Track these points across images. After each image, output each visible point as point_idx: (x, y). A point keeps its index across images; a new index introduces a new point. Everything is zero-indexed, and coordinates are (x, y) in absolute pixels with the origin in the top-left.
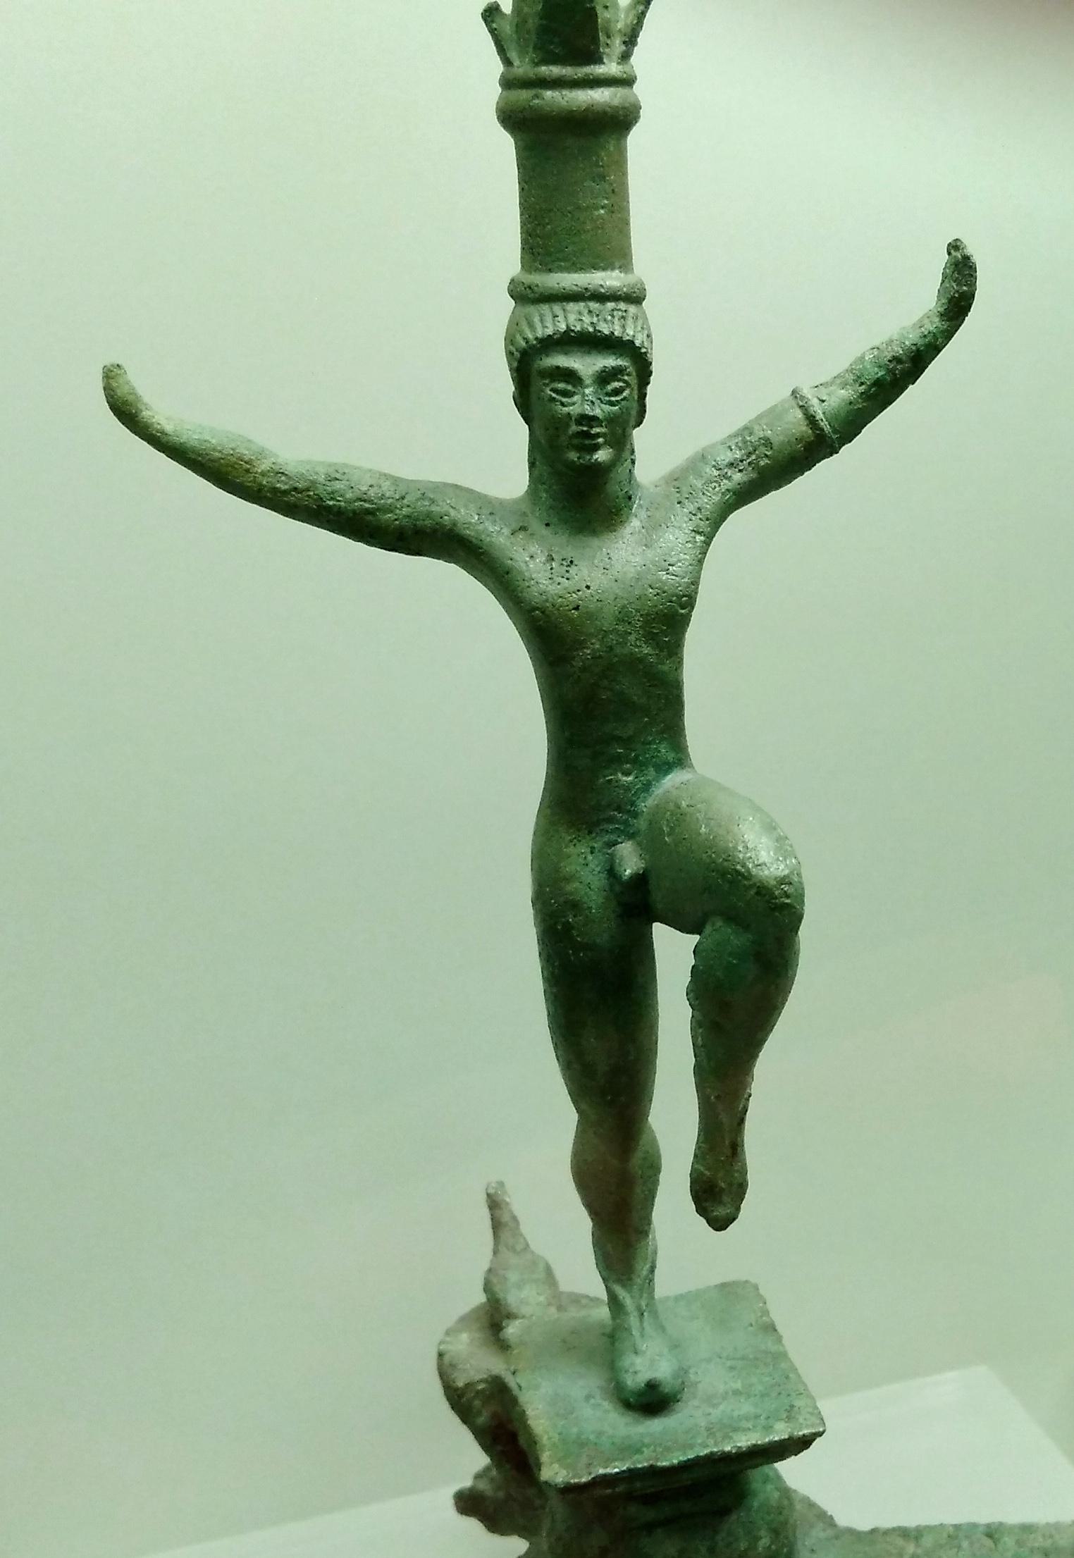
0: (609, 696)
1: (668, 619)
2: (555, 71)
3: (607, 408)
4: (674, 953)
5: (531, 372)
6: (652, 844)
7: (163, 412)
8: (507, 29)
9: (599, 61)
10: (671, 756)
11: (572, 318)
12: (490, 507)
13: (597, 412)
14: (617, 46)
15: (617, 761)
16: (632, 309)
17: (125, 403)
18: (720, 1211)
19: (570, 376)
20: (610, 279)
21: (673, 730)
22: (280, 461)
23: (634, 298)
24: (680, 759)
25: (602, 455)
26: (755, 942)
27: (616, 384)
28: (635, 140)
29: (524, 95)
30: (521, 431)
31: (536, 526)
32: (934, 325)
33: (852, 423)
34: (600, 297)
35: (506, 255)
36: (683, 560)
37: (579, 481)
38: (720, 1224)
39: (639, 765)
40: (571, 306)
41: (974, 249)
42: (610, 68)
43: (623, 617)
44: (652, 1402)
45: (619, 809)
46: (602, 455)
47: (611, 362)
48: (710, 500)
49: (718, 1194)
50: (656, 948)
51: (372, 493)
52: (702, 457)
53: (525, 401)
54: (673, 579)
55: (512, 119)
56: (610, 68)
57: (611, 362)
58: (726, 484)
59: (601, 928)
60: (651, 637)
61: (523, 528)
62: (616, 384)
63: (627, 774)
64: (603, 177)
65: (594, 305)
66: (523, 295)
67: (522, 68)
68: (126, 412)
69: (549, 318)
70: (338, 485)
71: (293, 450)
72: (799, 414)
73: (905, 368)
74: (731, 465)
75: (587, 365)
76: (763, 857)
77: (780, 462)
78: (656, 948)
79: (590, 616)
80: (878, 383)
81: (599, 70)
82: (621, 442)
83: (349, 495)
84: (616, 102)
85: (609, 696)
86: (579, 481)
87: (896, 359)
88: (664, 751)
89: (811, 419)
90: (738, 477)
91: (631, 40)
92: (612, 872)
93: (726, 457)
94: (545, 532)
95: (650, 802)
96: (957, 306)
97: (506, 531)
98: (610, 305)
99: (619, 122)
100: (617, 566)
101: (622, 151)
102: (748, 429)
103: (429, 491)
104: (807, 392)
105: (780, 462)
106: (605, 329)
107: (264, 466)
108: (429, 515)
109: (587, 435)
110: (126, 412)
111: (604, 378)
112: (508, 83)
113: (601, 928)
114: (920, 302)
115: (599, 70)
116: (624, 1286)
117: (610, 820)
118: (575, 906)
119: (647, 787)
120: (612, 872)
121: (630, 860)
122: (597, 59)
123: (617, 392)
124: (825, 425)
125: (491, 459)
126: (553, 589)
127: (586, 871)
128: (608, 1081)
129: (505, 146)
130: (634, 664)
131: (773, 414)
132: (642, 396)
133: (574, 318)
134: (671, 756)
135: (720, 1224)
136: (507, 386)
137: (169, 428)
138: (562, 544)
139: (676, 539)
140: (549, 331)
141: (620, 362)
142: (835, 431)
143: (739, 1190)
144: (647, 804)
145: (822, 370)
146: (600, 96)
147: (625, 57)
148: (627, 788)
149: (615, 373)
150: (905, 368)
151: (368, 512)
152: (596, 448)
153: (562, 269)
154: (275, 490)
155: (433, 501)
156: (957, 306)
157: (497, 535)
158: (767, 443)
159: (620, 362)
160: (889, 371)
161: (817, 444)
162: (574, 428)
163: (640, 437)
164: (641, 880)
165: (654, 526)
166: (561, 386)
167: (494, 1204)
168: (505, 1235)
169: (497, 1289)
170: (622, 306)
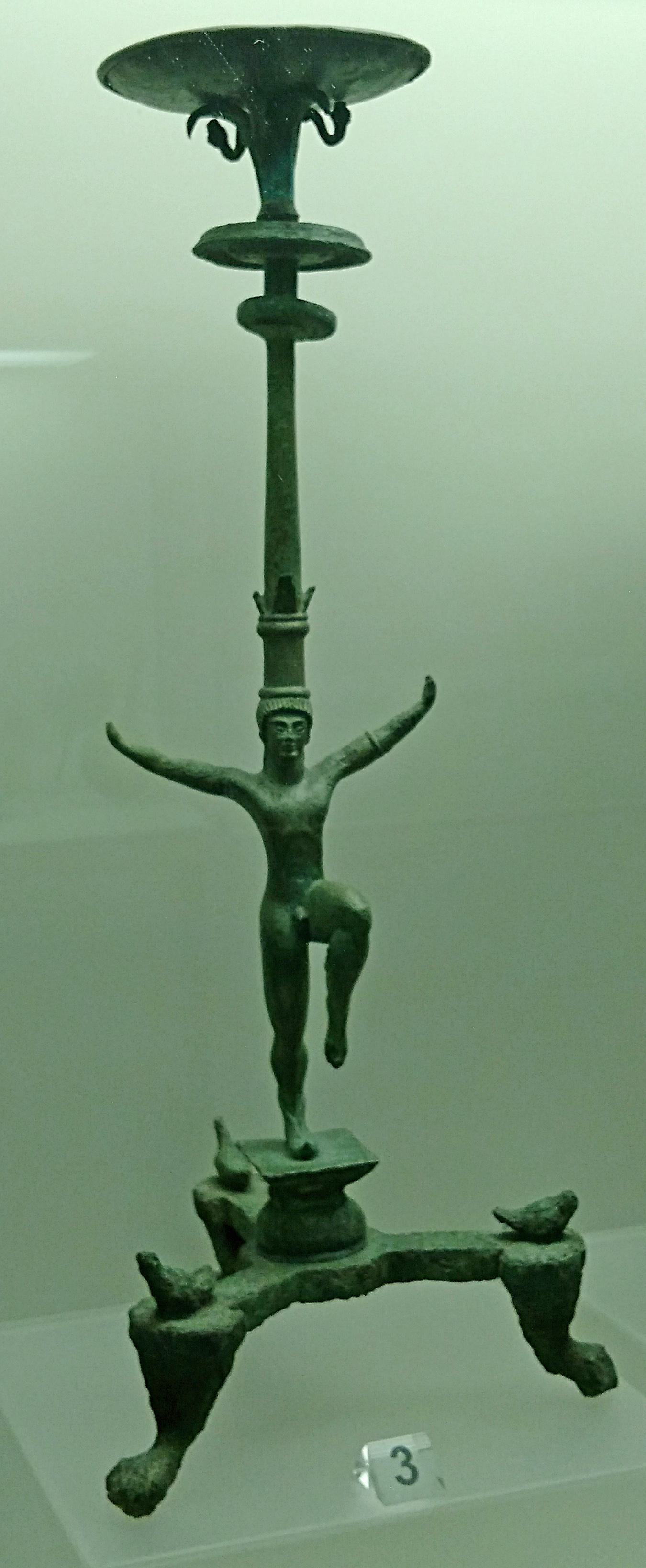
0: (292, 847)
1: (318, 816)
2: (280, 616)
4: (317, 953)
5: (267, 724)
6: (311, 906)
7: (127, 740)
8: (262, 601)
11: (285, 703)
12: (248, 776)
14: (302, 606)
16: (306, 700)
18: (338, 1059)
19: (283, 725)
21: (318, 863)
23: (306, 696)
24: (319, 875)
25: (294, 753)
26: (350, 936)
28: (307, 639)
29: (267, 625)
30: (262, 745)
31: (267, 782)
32: (419, 708)
33: (388, 745)
35: (259, 682)
36: (323, 795)
37: (283, 765)
38: (337, 1065)
41: (436, 679)
42: (300, 614)
43: (300, 817)
44: (307, 1153)
46: (294, 753)
47: (298, 719)
48: (334, 772)
49: (335, 1052)
50: (310, 944)
53: (263, 736)
54: (320, 802)
55: (262, 632)
56: (300, 614)
57: (298, 719)
58: (340, 768)
59: (288, 939)
65: (292, 698)
66: (263, 695)
67: (267, 614)
68: (114, 740)
69: (270, 704)
71: (172, 753)
75: (289, 720)
76: (357, 904)
77: (359, 760)
78: (310, 944)
82: (300, 750)
85: (292, 847)
86: (283, 765)
87: (406, 720)
88: (315, 871)
89: (372, 742)
90: (344, 765)
91: (306, 604)
92: (294, 918)
93: (339, 757)
94: (270, 785)
95: (310, 889)
96: (429, 700)
100: (298, 796)
101: (302, 643)
102: (347, 747)
103: (223, 771)
104: (371, 732)
105: (359, 760)
106: (297, 707)
107: (163, 760)
110: (114, 740)
111: (295, 725)
112: (261, 620)
113: (288, 939)
114: (416, 699)
116: (293, 1115)
118: (280, 933)
120: (294, 918)
121: (302, 913)
122: (294, 611)
123: (300, 730)
124: (378, 744)
125: (248, 758)
127: (283, 918)
128: (287, 1016)
129: (260, 641)
130: (305, 834)
131: (358, 741)
132: (308, 733)
133: (284, 703)
135: (337, 1065)
136: (257, 730)
139: (321, 786)
140: (276, 708)
143: (344, 1053)
144: (308, 891)
145: (377, 726)
146: (296, 624)
147: (305, 611)
156: (429, 700)
157: (252, 787)
158: (355, 751)
161: (376, 752)
162: (284, 743)
163: (307, 748)
164: (305, 921)
165: (310, 784)
166: (280, 728)
167: (218, 1127)
168: (224, 1140)
169: (223, 1161)
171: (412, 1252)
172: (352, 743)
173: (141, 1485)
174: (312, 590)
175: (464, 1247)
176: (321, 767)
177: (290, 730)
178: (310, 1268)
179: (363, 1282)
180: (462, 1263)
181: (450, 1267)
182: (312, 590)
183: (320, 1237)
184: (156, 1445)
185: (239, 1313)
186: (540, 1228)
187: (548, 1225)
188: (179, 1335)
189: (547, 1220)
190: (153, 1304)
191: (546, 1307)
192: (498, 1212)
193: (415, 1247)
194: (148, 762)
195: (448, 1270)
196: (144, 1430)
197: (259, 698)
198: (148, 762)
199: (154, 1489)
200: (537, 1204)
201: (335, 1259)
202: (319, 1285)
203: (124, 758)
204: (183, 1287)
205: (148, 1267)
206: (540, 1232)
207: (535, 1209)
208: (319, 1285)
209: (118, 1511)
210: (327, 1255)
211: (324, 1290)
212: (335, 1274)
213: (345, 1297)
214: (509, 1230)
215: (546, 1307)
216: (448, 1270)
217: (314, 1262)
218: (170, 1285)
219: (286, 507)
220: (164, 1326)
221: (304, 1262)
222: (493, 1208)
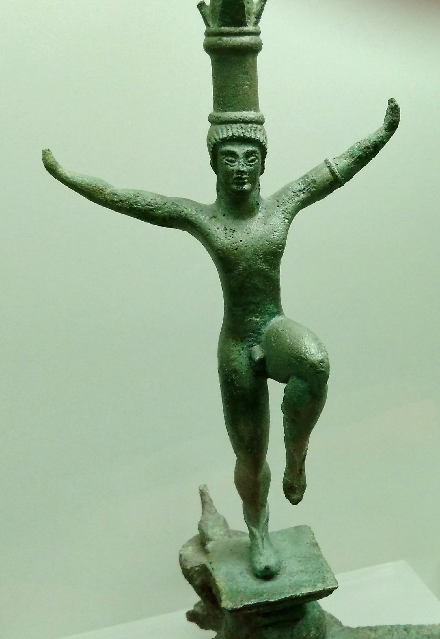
0: (250, 286)
1: (274, 254)
2: (228, 29)
3: (249, 167)
4: (276, 391)
5: (218, 152)
6: (267, 346)
7: (67, 169)
8: (208, 12)
9: (245, 25)
10: (275, 310)
11: (234, 130)
12: (201, 208)
13: (245, 169)
14: (253, 19)
15: (253, 312)
16: (259, 127)
17: (51, 165)
18: (295, 497)
19: (234, 154)
20: (250, 115)
21: (276, 299)
22: (115, 189)
23: (260, 122)
24: (279, 311)
25: (247, 187)
27: (252, 158)
28: (260, 57)
29: (215, 39)
30: (213, 177)
31: (220, 216)
32: (382, 133)
33: (349, 174)
34: (246, 122)
35: (207, 105)
36: (280, 230)
37: (237, 197)
38: (295, 502)
39: (262, 314)
40: (234, 126)
41: (399, 102)
42: (250, 28)
43: (255, 253)
44: (267, 575)
45: (254, 332)
46: (247, 187)
47: (250, 148)
48: (291, 205)
49: (294, 490)
50: (269, 389)
51: (152, 202)
52: (288, 188)
53: (215, 165)
54: (276, 238)
55: (210, 49)
56: (250, 28)
57: (250, 148)
58: (297, 199)
59: (246, 381)
60: (267, 261)
61: (214, 217)
62: (252, 158)
63: (257, 317)
64: (247, 73)
65: (243, 125)
66: (214, 121)
67: (214, 28)
68: (52, 169)
69: (225, 131)
70: (138, 199)
71: (120, 185)
72: (327, 170)
73: (371, 151)
74: (300, 191)
75: (240, 150)
76: (313, 351)
77: (319, 189)
78: (269, 389)
79: (242, 253)
80: (360, 157)
81: (246, 29)
82: (254, 181)
83: (143, 203)
84: (252, 42)
85: (250, 286)
86: (237, 197)
87: (367, 147)
88: (272, 308)
89: (332, 172)
90: (302, 196)
91: (258, 16)
92: (251, 358)
93: (297, 187)
94: (223, 218)
95: (266, 329)
96: (392, 126)
97: (207, 218)
98: (250, 125)
99: (254, 50)
100: (253, 232)
101: (255, 62)
102: (306, 176)
103: (176, 202)
104: (330, 161)
105: (319, 189)
106: (248, 135)
107: (108, 191)
108: (176, 211)
109: (240, 178)
110: (52, 169)
111: (247, 155)
112: (208, 34)
113: (246, 381)
114: (377, 124)
115: (246, 29)
116: (256, 527)
117: (250, 336)
118: (236, 372)
119: (265, 323)
120: (251, 358)
121: (258, 353)
122: (245, 24)
123: (253, 161)
124: (338, 174)
125: (201, 188)
126: (226, 242)
127: (240, 357)
128: (249, 444)
129: (207, 60)
130: (260, 272)
131: (317, 170)
132: (263, 162)
133: (235, 130)
134: (275, 310)
135: (295, 502)
136: (208, 158)
137: (69, 175)
138: (230, 223)
139: (277, 221)
140: (225, 136)
141: (254, 149)
142: (342, 177)
143: (303, 488)
144: (265, 330)
145: (337, 152)
146: (246, 39)
147: (256, 23)
148: (257, 323)
149: (252, 153)
150: (371, 151)
151: (151, 210)
152: (244, 184)
153: (230, 111)
154: (113, 201)
155: (177, 206)
156: (392, 126)
157: (204, 219)
158: (314, 182)
159: (254, 149)
160: (364, 152)
161: (335, 182)
162: (235, 176)
163: (262, 179)
164: (262, 361)
165: (268, 216)
166: (230, 158)
167: (202, 494)
168: (207, 507)
169: (204, 528)
170: (255, 125)
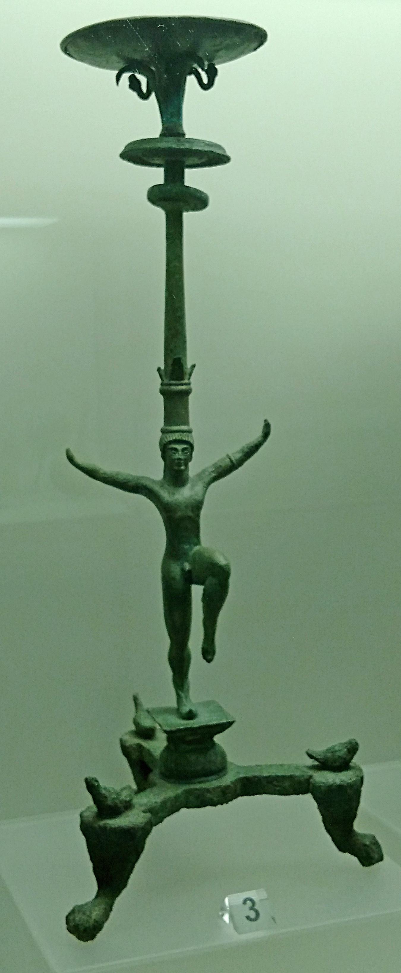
0: (181, 526)
1: (197, 506)
2: (174, 382)
4: (197, 591)
5: (166, 449)
6: (193, 562)
7: (79, 459)
8: (163, 373)
11: (177, 436)
12: (154, 481)
14: (187, 376)
16: (190, 434)
18: (210, 657)
19: (176, 450)
21: (198, 535)
23: (190, 432)
24: (198, 543)
25: (183, 468)
28: (191, 397)
29: (166, 388)
30: (162, 463)
31: (166, 485)
32: (260, 439)
33: (241, 462)
35: (161, 423)
36: (200, 493)
37: (176, 475)
38: (209, 661)
41: (270, 422)
42: (186, 381)
43: (187, 507)
44: (191, 715)
46: (183, 468)
47: (185, 446)
48: (207, 479)
49: (208, 653)
50: (193, 586)
53: (164, 457)
54: (199, 498)
55: (162, 392)
56: (186, 381)
57: (185, 446)
58: (211, 476)
59: (179, 583)
65: (181, 433)
66: (163, 431)
67: (166, 381)
68: (71, 459)
69: (168, 437)
71: (107, 467)
75: (179, 447)
76: (221, 561)
77: (223, 472)
78: (193, 586)
82: (186, 465)
85: (181, 526)
86: (176, 475)
87: (252, 447)
88: (196, 540)
89: (231, 461)
90: (214, 475)
91: (190, 375)
92: (183, 570)
93: (210, 470)
94: (168, 487)
95: (193, 552)
96: (266, 434)
100: (185, 494)
101: (188, 399)
102: (216, 463)
103: (138, 478)
104: (230, 454)
105: (223, 472)
106: (184, 439)
107: (101, 472)
110: (71, 459)
111: (183, 450)
112: (162, 384)
113: (179, 583)
114: (258, 434)
116: (182, 692)
118: (174, 579)
120: (183, 570)
121: (187, 566)
122: (183, 379)
123: (186, 453)
124: (234, 462)
125: (154, 470)
127: (176, 570)
128: (178, 630)
129: (161, 398)
130: (189, 518)
131: (222, 460)
132: (191, 455)
133: (177, 436)
135: (209, 661)
136: (159, 453)
139: (199, 488)
140: (171, 439)
143: (214, 653)
144: (191, 553)
145: (234, 451)
146: (184, 387)
147: (189, 379)
156: (266, 434)
157: (157, 488)
158: (221, 466)
161: (233, 466)
162: (176, 461)
163: (190, 464)
164: (190, 571)
165: (193, 486)
166: (173, 452)
167: (136, 699)
168: (139, 707)
169: (139, 720)
171: (256, 777)
172: (218, 461)
173: (88, 921)
174: (194, 366)
175: (288, 774)
176: (199, 476)
177: (180, 453)
178: (192, 787)
179: (225, 796)
180: (287, 784)
181: (279, 786)
182: (194, 366)
183: (199, 768)
184: (97, 897)
185: (148, 815)
186: (335, 762)
187: (340, 760)
188: (111, 828)
189: (339, 757)
190: (95, 809)
191: (339, 811)
192: (309, 752)
193: (257, 774)
194: (92, 473)
195: (278, 788)
196: (89, 887)
197: (161, 433)
198: (92, 473)
199: (95, 924)
200: (333, 747)
201: (208, 781)
202: (198, 797)
203: (77, 470)
204: (114, 799)
205: (92, 787)
206: (335, 765)
207: (332, 750)
208: (198, 797)
209: (73, 938)
210: (203, 779)
211: (201, 801)
212: (208, 791)
213: (214, 805)
214: (316, 763)
215: (339, 811)
216: (278, 788)
217: (195, 783)
218: (106, 797)
219: (178, 314)
220: (102, 823)
221: (189, 783)
222: (306, 750)
